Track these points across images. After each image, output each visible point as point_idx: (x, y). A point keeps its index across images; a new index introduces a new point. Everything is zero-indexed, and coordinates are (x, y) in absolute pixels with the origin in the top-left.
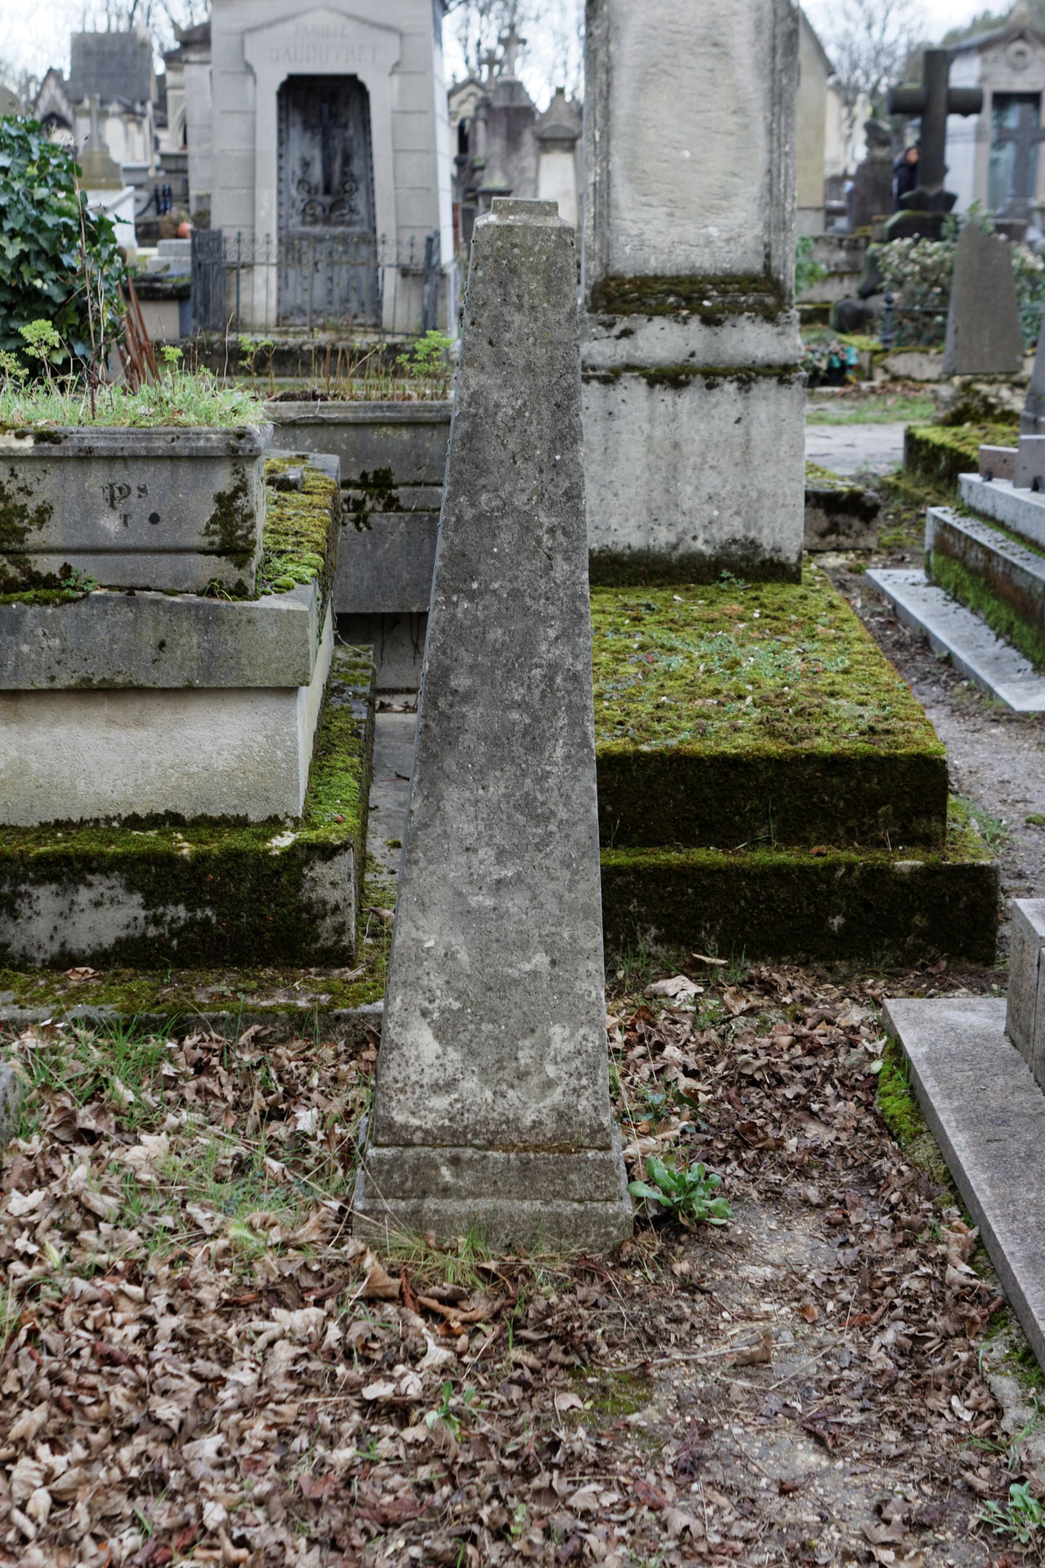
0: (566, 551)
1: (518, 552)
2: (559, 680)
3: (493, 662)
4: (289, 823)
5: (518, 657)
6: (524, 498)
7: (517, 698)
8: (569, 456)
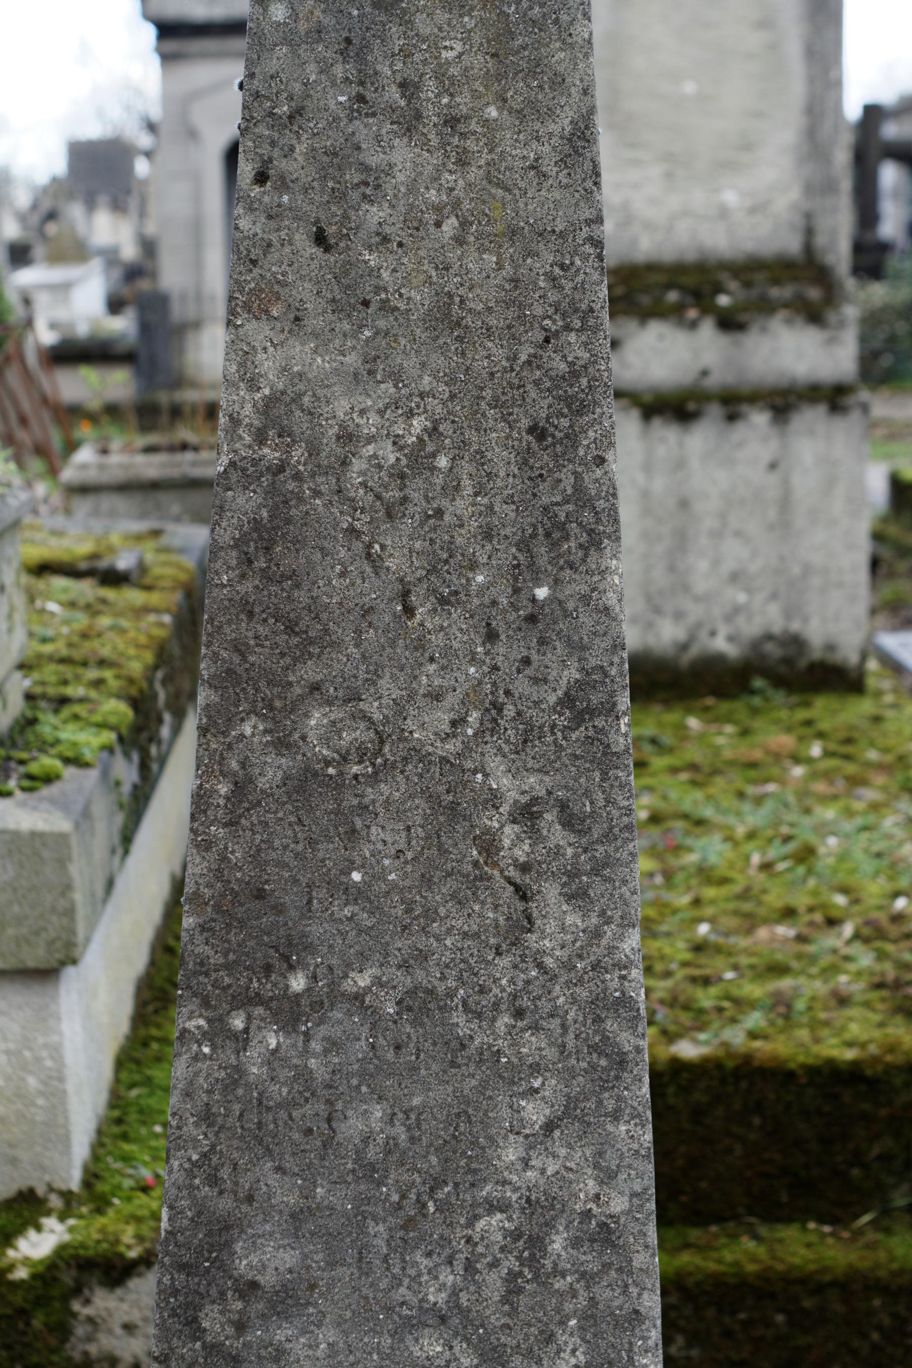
0: (573, 874)
1: (427, 881)
2: (557, 1244)
3: (360, 1200)
4: (55, 1202)
5: (436, 1184)
6: (441, 718)
7: (436, 1297)
8: (576, 586)
